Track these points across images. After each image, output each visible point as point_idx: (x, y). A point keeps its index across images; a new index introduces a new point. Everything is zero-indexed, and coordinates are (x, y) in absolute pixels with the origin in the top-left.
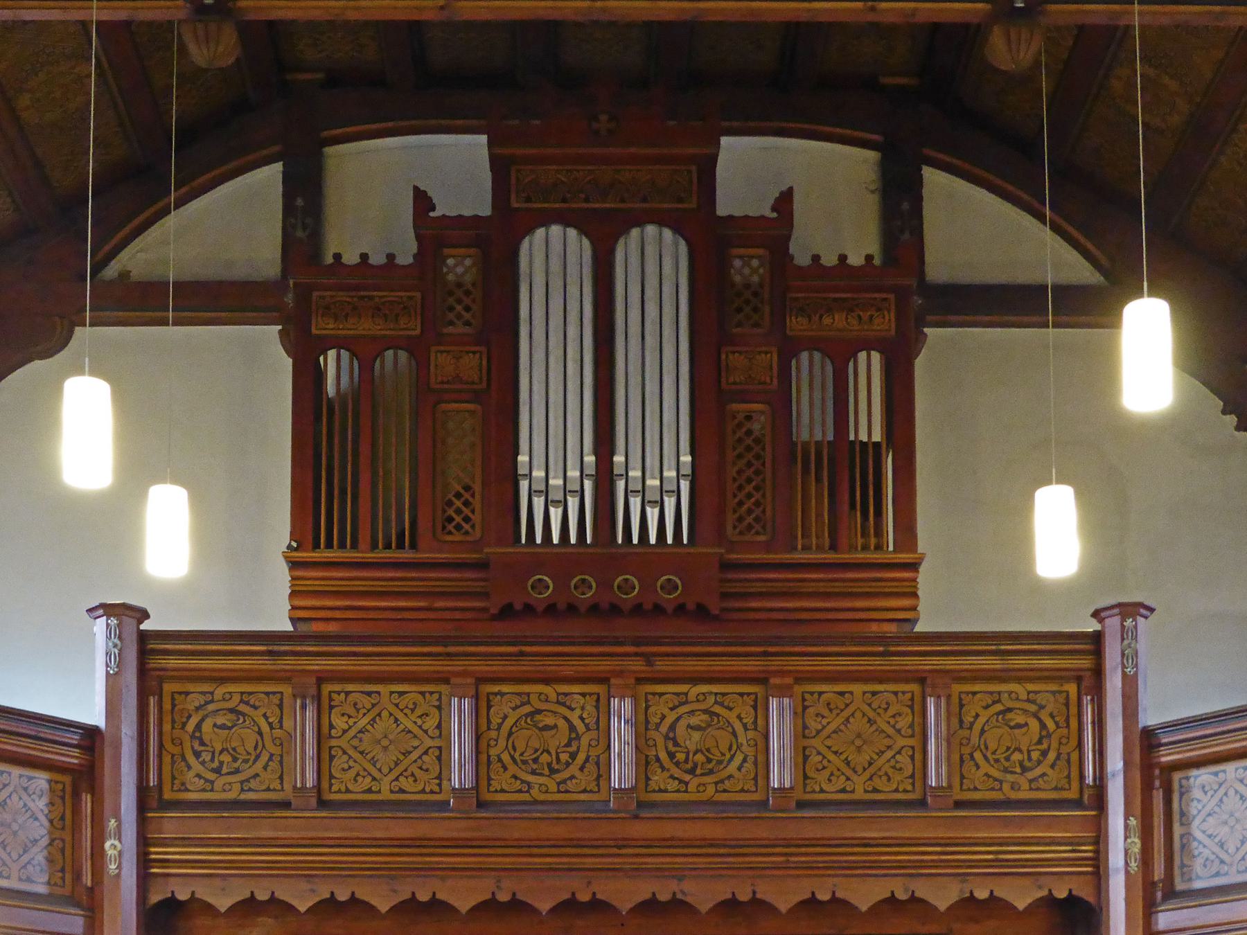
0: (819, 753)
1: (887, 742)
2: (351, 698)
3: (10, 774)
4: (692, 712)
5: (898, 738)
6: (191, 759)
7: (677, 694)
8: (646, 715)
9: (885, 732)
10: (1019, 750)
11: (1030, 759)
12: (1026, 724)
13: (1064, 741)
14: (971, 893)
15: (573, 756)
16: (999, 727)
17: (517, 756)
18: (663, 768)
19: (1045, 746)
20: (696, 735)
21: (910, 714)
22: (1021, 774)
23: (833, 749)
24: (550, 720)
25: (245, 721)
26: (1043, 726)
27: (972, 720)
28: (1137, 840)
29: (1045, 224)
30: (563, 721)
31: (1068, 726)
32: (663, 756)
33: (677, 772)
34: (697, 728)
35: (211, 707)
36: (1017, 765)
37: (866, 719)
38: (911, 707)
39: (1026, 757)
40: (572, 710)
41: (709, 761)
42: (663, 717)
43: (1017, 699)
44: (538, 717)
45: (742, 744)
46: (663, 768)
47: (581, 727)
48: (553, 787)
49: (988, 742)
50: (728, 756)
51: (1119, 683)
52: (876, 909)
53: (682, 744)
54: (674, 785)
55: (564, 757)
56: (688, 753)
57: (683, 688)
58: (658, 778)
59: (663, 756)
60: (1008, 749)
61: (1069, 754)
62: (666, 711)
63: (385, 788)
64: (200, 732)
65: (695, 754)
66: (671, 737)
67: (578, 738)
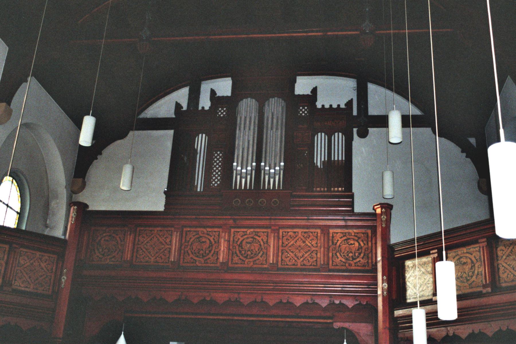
0: (287, 252)
1: (309, 249)
2: (289, 233)
3: (36, 254)
4: (248, 238)
5: (312, 247)
6: (96, 251)
7: (244, 232)
8: (233, 238)
9: (512, 249)
10: (351, 252)
11: (355, 256)
12: (354, 244)
13: (334, 249)
14: (333, 301)
15: (210, 251)
16: (345, 244)
17: (193, 251)
18: (237, 256)
19: (360, 251)
20: (248, 245)
21: (316, 240)
22: (352, 261)
23: (291, 251)
24: (204, 240)
25: (256, 241)
26: (360, 244)
27: (336, 242)
28: (386, 284)
29: (393, 91)
30: (208, 240)
31: (368, 245)
32: (238, 252)
33: (241, 257)
34: (250, 243)
35: (246, 237)
36: (351, 257)
37: (302, 241)
38: (317, 237)
39: (354, 255)
40: (211, 236)
41: (252, 254)
42: (239, 239)
43: (351, 235)
44: (201, 239)
45: (262, 249)
46: (237, 256)
47: (213, 243)
48: (203, 261)
49: (342, 249)
50: (258, 252)
51: (380, 230)
52: (276, 306)
53: (244, 248)
54: (240, 262)
55: (357, 254)
56: (245, 251)
57: (245, 230)
58: (236, 259)
59: (238, 252)
60: (348, 252)
61: (368, 254)
62: (239, 237)
63: (299, 265)
64: (242, 244)
65: (248, 251)
66: (240, 245)
67: (212, 246)
